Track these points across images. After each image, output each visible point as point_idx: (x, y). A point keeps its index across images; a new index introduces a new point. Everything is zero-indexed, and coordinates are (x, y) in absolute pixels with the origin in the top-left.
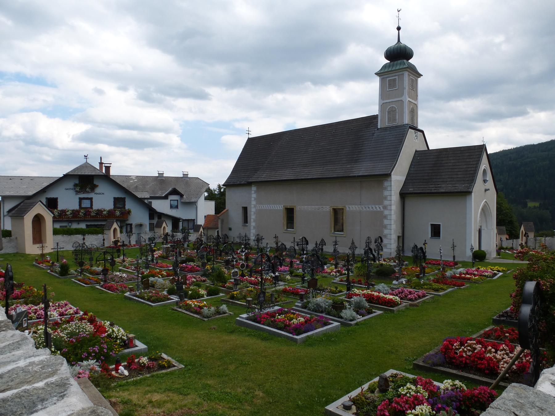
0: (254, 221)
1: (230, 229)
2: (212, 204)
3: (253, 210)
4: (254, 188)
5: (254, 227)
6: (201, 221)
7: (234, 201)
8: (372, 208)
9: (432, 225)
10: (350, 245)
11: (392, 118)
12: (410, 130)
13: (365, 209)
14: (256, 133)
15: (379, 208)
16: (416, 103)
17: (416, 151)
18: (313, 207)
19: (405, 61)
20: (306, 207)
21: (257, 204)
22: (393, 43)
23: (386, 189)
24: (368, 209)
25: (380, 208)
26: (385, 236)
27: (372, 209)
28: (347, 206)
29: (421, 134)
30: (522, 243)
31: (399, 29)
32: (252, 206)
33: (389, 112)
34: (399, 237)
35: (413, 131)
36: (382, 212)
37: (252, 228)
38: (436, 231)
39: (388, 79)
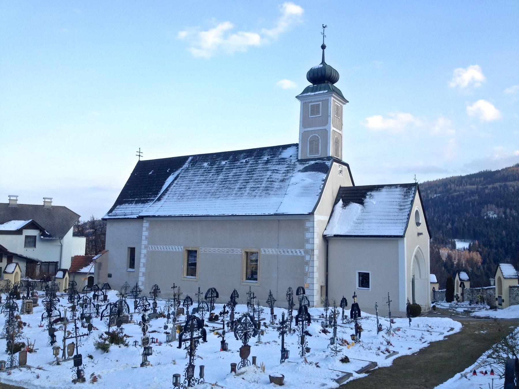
0: (144, 266)
1: (110, 276)
2: (82, 241)
3: (144, 251)
4: (146, 224)
5: (144, 274)
6: (66, 264)
7: (116, 240)
8: (292, 252)
9: (359, 273)
10: (267, 297)
11: (314, 148)
12: (334, 163)
13: (283, 254)
14: (147, 157)
15: (299, 252)
16: (340, 132)
17: (340, 187)
18: (221, 249)
19: (330, 85)
20: (212, 249)
21: (148, 244)
22: (317, 64)
23: (307, 230)
24: (287, 254)
25: (300, 252)
26: (305, 286)
27: (291, 254)
28: (262, 249)
29: (346, 167)
30: (457, 295)
31: (323, 47)
32: (143, 247)
33: (310, 142)
34: (321, 287)
35: (338, 164)
36: (303, 258)
37: (141, 274)
38: (364, 280)
39: (310, 104)
